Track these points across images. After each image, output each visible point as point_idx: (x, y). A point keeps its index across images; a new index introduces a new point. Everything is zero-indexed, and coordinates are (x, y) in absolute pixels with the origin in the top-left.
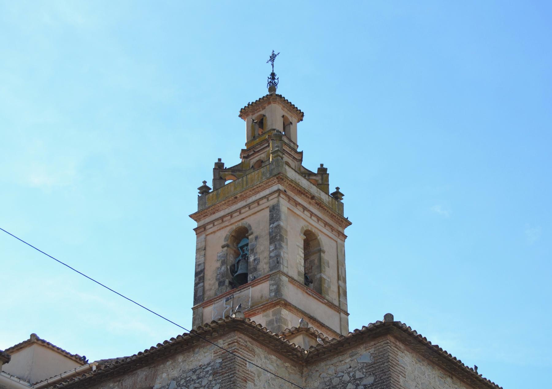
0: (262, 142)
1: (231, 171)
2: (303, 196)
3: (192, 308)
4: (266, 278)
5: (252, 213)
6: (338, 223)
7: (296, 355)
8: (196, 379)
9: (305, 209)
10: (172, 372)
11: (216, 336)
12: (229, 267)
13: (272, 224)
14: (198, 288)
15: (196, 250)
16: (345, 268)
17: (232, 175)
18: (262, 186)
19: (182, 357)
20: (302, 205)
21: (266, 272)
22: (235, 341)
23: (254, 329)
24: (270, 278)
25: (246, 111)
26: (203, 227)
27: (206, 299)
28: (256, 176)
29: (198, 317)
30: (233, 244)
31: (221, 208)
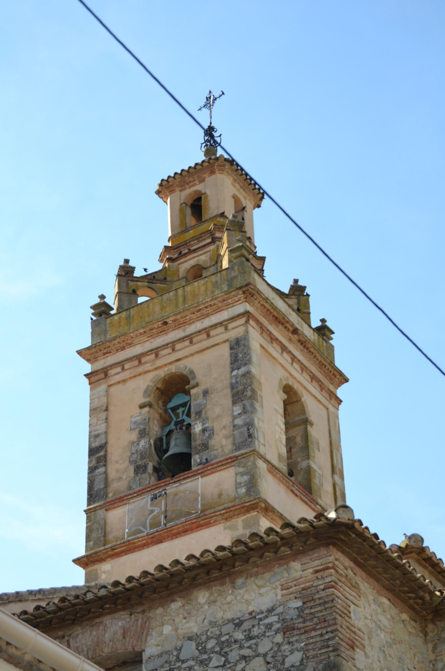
0: (202, 235)
1: (147, 281)
2: (280, 327)
3: (85, 511)
4: (228, 463)
5: (197, 350)
6: (328, 378)
7: (422, 598)
8: (242, 640)
9: (284, 348)
10: (185, 623)
11: (286, 553)
12: (152, 442)
13: (235, 370)
14: (96, 475)
15: (90, 410)
16: (341, 455)
17: (149, 287)
18: (215, 304)
19: (207, 594)
20: (280, 342)
21: (227, 452)
22: (330, 565)
23: (365, 543)
24: (235, 462)
25: (170, 184)
26: (104, 372)
27: (110, 495)
28: (203, 288)
29: (95, 526)
30: (158, 403)
31: (137, 340)
